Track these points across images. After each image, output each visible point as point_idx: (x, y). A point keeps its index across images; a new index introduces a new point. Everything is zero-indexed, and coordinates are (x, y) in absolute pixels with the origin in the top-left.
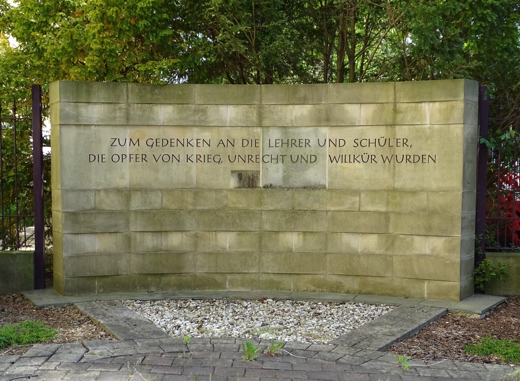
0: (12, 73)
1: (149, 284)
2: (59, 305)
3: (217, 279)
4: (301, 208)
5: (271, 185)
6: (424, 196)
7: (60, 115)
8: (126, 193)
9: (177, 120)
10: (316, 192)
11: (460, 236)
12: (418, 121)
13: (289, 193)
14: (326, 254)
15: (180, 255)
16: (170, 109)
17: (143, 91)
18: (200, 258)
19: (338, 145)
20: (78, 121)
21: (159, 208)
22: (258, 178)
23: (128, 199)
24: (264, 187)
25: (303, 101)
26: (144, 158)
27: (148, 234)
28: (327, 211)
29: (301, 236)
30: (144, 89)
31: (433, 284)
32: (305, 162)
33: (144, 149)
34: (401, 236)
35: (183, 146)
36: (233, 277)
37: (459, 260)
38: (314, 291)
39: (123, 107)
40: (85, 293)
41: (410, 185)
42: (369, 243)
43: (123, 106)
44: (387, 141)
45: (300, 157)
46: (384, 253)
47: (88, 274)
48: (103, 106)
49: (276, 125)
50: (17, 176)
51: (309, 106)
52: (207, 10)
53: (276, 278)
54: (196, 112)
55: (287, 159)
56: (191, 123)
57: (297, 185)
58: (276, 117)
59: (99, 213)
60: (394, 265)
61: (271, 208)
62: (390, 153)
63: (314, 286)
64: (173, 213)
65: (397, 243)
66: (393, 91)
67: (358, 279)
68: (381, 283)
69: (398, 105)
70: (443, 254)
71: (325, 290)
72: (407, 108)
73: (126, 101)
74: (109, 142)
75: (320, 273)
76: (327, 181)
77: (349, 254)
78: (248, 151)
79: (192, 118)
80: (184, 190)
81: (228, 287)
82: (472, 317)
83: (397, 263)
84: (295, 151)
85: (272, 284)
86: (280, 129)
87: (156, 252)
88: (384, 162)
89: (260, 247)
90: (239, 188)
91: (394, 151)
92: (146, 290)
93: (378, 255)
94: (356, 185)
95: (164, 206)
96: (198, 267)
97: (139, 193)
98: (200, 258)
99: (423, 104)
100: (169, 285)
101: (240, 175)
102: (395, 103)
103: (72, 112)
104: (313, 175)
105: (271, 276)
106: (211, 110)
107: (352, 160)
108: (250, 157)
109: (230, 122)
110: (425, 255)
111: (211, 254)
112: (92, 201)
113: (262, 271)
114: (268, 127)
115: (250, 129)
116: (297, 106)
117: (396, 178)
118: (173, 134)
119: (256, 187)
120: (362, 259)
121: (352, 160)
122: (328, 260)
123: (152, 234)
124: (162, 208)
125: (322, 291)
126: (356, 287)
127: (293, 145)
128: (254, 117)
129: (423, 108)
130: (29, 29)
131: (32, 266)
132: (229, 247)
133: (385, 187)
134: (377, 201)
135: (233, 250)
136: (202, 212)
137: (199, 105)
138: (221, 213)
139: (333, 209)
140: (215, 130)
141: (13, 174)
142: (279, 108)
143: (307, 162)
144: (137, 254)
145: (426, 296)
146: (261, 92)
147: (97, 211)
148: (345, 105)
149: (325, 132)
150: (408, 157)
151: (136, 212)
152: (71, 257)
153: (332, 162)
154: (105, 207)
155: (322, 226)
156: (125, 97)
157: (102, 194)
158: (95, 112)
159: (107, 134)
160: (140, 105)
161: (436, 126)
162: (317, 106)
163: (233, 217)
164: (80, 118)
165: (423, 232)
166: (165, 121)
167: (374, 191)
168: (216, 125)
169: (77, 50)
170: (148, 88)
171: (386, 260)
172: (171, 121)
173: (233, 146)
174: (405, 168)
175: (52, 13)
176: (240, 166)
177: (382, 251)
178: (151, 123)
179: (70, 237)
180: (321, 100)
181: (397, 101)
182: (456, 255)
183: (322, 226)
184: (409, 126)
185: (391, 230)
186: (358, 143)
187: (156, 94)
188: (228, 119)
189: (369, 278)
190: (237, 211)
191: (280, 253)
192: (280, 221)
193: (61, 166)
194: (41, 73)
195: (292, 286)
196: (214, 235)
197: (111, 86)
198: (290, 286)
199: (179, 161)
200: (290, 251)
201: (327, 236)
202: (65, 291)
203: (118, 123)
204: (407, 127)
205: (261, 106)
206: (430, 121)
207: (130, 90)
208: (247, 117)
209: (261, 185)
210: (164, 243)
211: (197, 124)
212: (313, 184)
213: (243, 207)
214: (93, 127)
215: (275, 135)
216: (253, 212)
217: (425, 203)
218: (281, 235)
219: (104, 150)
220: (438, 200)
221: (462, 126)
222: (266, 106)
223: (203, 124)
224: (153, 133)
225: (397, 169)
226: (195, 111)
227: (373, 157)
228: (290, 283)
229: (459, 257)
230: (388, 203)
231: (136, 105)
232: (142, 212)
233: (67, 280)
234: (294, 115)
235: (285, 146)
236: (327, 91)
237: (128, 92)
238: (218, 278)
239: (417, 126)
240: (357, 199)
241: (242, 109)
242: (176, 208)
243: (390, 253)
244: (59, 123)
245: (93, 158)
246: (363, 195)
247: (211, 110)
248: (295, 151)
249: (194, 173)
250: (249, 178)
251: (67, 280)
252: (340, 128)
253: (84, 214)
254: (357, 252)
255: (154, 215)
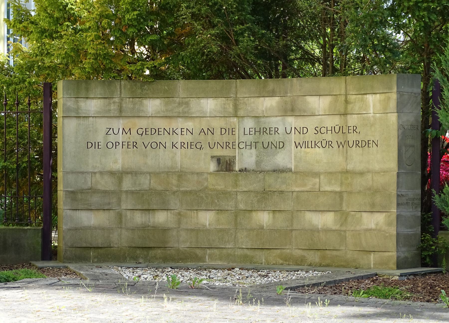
0: (26, 74)
1: (138, 256)
2: (56, 267)
3: (198, 253)
4: (270, 189)
5: (246, 169)
6: (369, 176)
7: (63, 108)
8: (118, 175)
9: (164, 112)
10: (284, 175)
11: (396, 211)
12: (364, 111)
13: (261, 176)
14: (292, 230)
15: (165, 230)
16: (157, 102)
17: (134, 87)
18: (183, 234)
19: (301, 133)
20: (78, 113)
21: (148, 189)
22: (234, 163)
23: (120, 181)
24: (240, 171)
25: (272, 94)
26: (135, 145)
27: (138, 211)
28: (292, 192)
29: (271, 215)
30: (135, 85)
31: (378, 255)
32: (275, 148)
33: (135, 137)
34: (353, 213)
35: (169, 134)
36: (212, 251)
37: (395, 232)
38: (282, 264)
39: (117, 101)
40: (81, 261)
41: (360, 167)
42: (326, 220)
43: (117, 100)
44: (341, 128)
45: (270, 143)
46: (339, 229)
47: (84, 245)
48: (99, 100)
49: (250, 115)
50: (30, 162)
51: (277, 98)
52: (181, 17)
53: (249, 253)
54: (180, 104)
55: (260, 145)
56: (176, 115)
57: (268, 168)
58: (249, 108)
59: (94, 192)
60: (347, 239)
61: (245, 189)
62: (344, 138)
63: (281, 259)
64: (159, 193)
65: (349, 219)
66: (344, 84)
67: (319, 253)
68: (337, 256)
69: (348, 96)
70: (385, 228)
71: (291, 263)
72: (355, 99)
73: (119, 96)
74: (104, 131)
75: (287, 247)
76: (293, 164)
77: (311, 230)
78: (226, 138)
79: (177, 110)
80: (169, 173)
81: (207, 260)
82: (394, 279)
83: (349, 237)
84: (266, 138)
85: (245, 258)
86: (253, 119)
87: (144, 228)
88: (339, 147)
89: (236, 224)
90: (218, 171)
91: (347, 137)
92: (135, 262)
93: (334, 231)
94: (317, 168)
95: (151, 187)
96: (182, 242)
97: (130, 176)
98: (183, 234)
99: (368, 96)
100: (155, 258)
101: (219, 160)
102: (346, 95)
103: (73, 106)
104: (282, 159)
105: (245, 250)
106: (193, 102)
107: (313, 146)
108: (228, 144)
109: (210, 112)
110: (371, 230)
111: (192, 230)
112: (89, 182)
113: (237, 246)
114: (243, 117)
115: (228, 119)
116: (267, 98)
117: (348, 161)
118: (160, 124)
119: (232, 171)
120: (321, 234)
121: (313, 146)
122: (294, 236)
123: (141, 211)
124: (150, 189)
125: (288, 264)
126: (317, 260)
127: (264, 133)
128: (230, 108)
129: (368, 99)
130: (42, 35)
131: (40, 240)
132: (209, 225)
133: (339, 169)
134: (333, 182)
135: (212, 227)
136: (185, 193)
137: (183, 98)
138: (201, 194)
139: (297, 189)
140: (197, 120)
141: (27, 159)
142: (252, 100)
143: (276, 148)
144: (127, 229)
145: (372, 266)
146: (236, 86)
147: (93, 191)
148: (307, 97)
149: (291, 121)
150: (357, 142)
151: (127, 192)
152: (69, 230)
153: (297, 148)
154: (100, 187)
155: (288, 205)
156: (119, 93)
157: (98, 176)
158: (92, 105)
159: (103, 124)
160: (131, 99)
161: (378, 115)
162: (284, 98)
163: (212, 197)
164: (80, 111)
165: (368, 209)
166: (153, 113)
167: (331, 173)
168: (198, 116)
169: (78, 53)
170: (139, 84)
171: (341, 235)
172: (159, 112)
173: (213, 134)
174: (355, 152)
175: (61, 21)
176: (219, 152)
177: (337, 227)
178: (141, 115)
179: (69, 212)
180: (286, 93)
181: (348, 93)
182: (393, 228)
183: (288, 205)
184: (357, 115)
185: (344, 208)
186: (318, 131)
187: (146, 89)
188: (208, 110)
189: (327, 252)
190: (215, 192)
191: (252, 230)
192: (252, 201)
193: (63, 152)
194: (50, 72)
195: (264, 260)
196: (195, 214)
197: (106, 83)
198: (262, 260)
199: (165, 148)
200: (262, 228)
201: (292, 214)
202: (64, 259)
203: (112, 115)
204: (356, 115)
205: (236, 99)
206: (373, 110)
207: (122, 87)
208: (224, 108)
209: (237, 169)
210: (152, 220)
211: (181, 115)
212: (281, 168)
213: (221, 189)
214: (91, 119)
215: (249, 124)
216: (230, 193)
217: (371, 183)
218: (254, 214)
219: (100, 138)
220: (380, 180)
221: (396, 114)
222: (241, 98)
223: (187, 115)
224: (143, 123)
225: (349, 153)
226: (179, 104)
227: (330, 143)
228: (261, 257)
229: (396, 230)
230: (341, 184)
231: (128, 99)
232: (132, 192)
233: (66, 249)
234: (265, 106)
235: (257, 134)
236: (292, 85)
237: (122, 87)
238: (198, 252)
239: (363, 115)
240: (317, 180)
241: (221, 101)
242: (162, 189)
243: (343, 228)
244: (62, 116)
245: (90, 145)
246: (322, 177)
247: (193, 102)
248: (266, 138)
249: (178, 158)
250: (227, 162)
251: (66, 249)
252: (304, 117)
253: (81, 193)
254: (318, 228)
255: (143, 195)
